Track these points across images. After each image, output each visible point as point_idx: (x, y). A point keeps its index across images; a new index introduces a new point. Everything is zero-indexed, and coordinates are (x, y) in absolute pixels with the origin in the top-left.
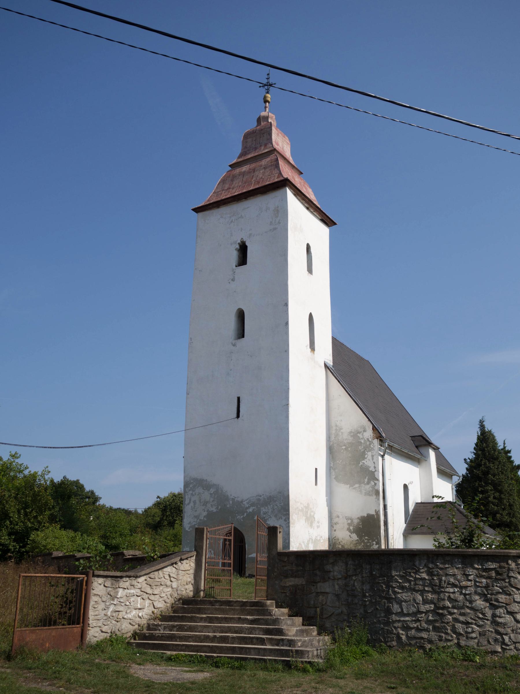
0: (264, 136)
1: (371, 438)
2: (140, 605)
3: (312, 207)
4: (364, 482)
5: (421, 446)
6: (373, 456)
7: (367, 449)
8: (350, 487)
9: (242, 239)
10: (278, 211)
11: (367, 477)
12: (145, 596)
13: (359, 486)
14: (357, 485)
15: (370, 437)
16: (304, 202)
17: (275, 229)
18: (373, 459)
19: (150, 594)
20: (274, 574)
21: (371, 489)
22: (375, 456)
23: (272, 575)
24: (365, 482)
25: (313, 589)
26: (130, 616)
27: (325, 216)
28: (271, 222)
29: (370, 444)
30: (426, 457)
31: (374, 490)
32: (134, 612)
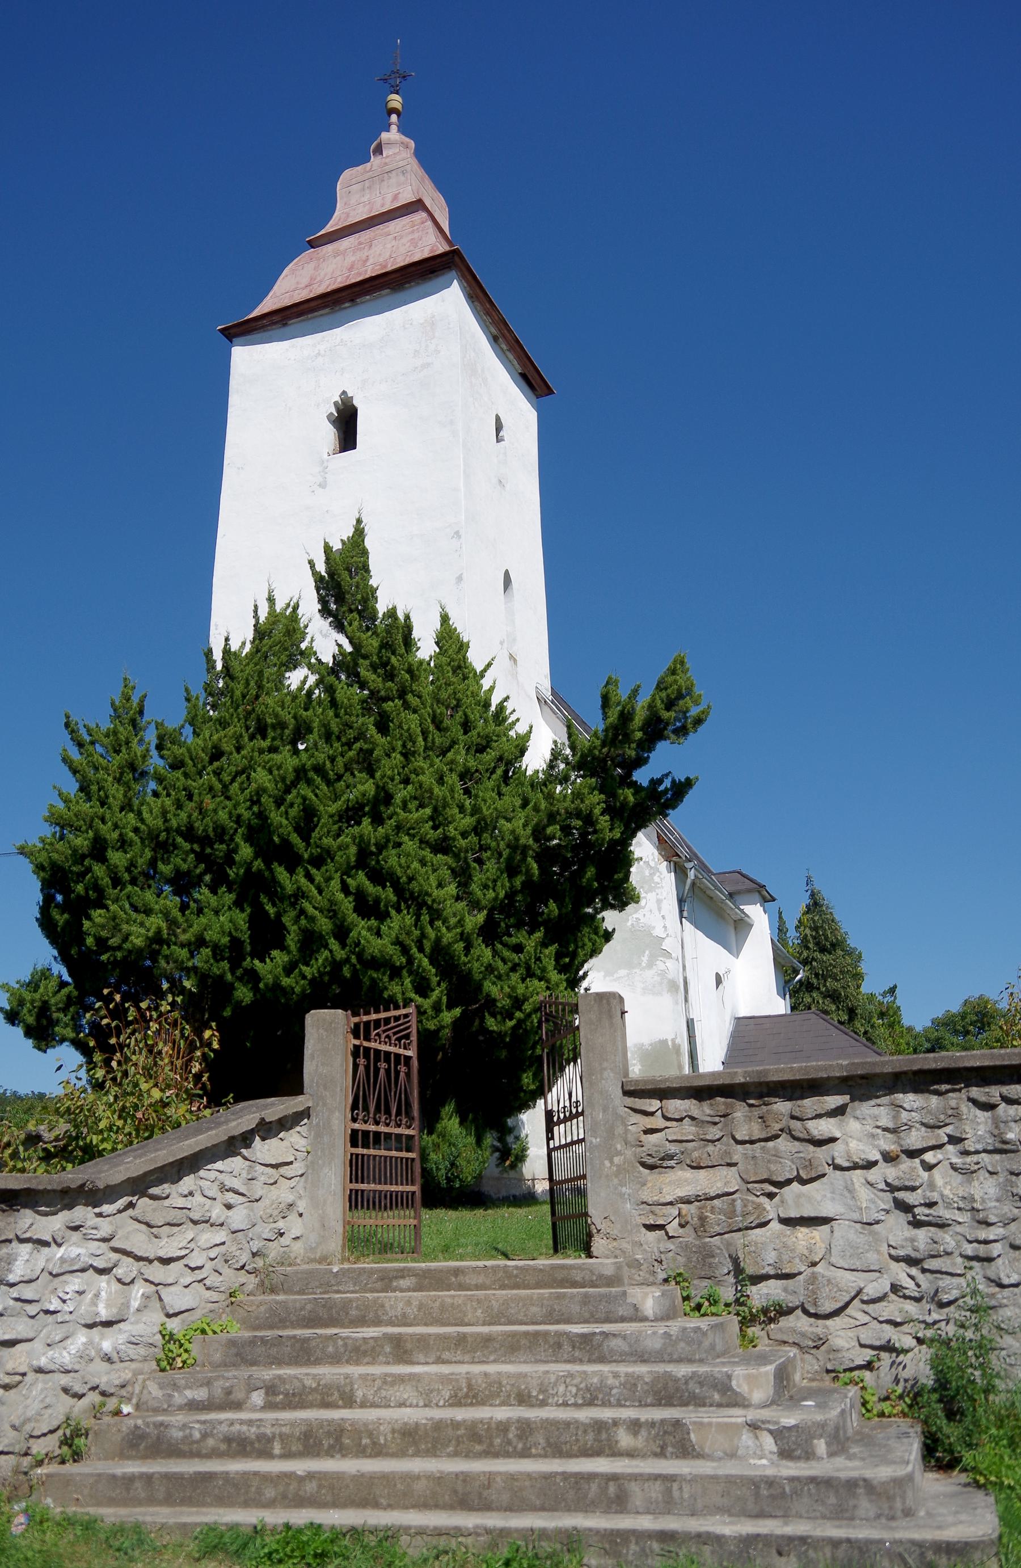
0: (390, 178)
1: (653, 860)
2: (108, 1306)
3: (504, 336)
4: (640, 964)
5: (739, 892)
6: (659, 902)
7: (646, 887)
8: (605, 977)
9: (344, 393)
10: (433, 324)
11: (647, 952)
12: (126, 1268)
13: (628, 975)
14: (623, 972)
15: (651, 858)
16: (488, 319)
17: (427, 365)
18: (660, 909)
19: (151, 1261)
20: (611, 1162)
21: (657, 978)
22: (665, 901)
23: (607, 1163)
24: (644, 964)
25: (768, 1208)
26: (65, 1356)
27: (532, 369)
28: (416, 351)
29: (652, 875)
30: (742, 926)
31: (665, 981)
32: (82, 1338)
